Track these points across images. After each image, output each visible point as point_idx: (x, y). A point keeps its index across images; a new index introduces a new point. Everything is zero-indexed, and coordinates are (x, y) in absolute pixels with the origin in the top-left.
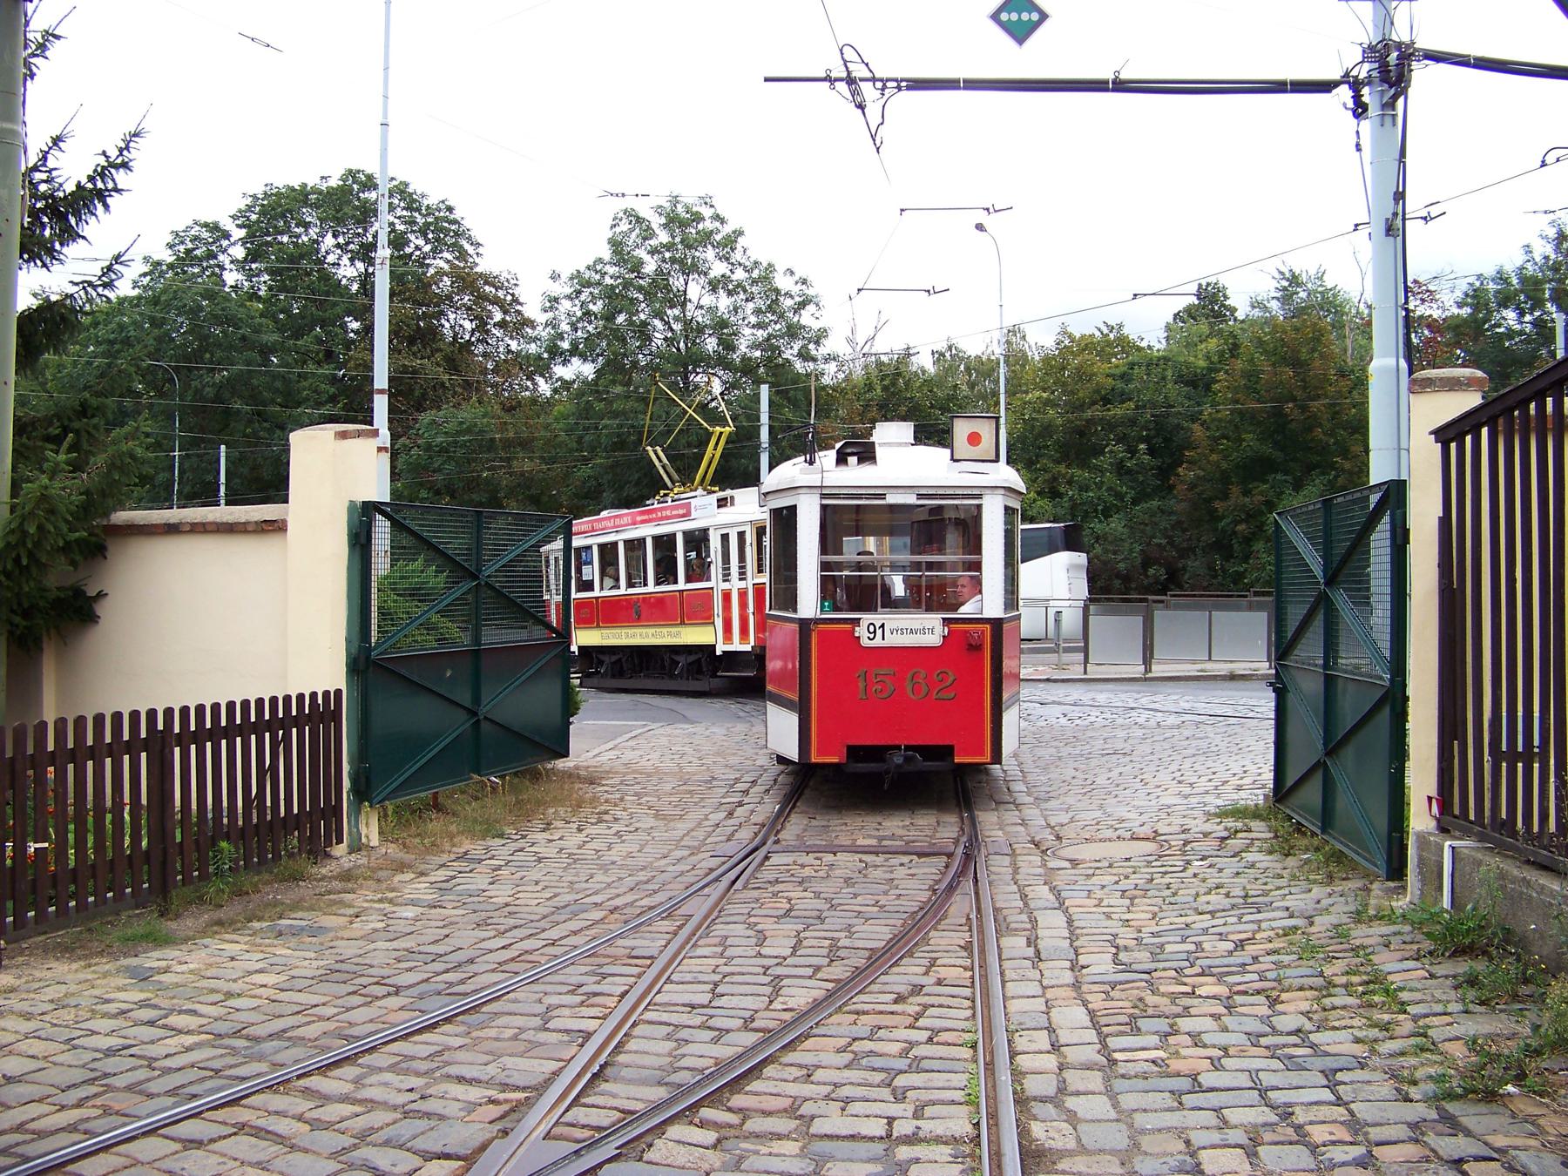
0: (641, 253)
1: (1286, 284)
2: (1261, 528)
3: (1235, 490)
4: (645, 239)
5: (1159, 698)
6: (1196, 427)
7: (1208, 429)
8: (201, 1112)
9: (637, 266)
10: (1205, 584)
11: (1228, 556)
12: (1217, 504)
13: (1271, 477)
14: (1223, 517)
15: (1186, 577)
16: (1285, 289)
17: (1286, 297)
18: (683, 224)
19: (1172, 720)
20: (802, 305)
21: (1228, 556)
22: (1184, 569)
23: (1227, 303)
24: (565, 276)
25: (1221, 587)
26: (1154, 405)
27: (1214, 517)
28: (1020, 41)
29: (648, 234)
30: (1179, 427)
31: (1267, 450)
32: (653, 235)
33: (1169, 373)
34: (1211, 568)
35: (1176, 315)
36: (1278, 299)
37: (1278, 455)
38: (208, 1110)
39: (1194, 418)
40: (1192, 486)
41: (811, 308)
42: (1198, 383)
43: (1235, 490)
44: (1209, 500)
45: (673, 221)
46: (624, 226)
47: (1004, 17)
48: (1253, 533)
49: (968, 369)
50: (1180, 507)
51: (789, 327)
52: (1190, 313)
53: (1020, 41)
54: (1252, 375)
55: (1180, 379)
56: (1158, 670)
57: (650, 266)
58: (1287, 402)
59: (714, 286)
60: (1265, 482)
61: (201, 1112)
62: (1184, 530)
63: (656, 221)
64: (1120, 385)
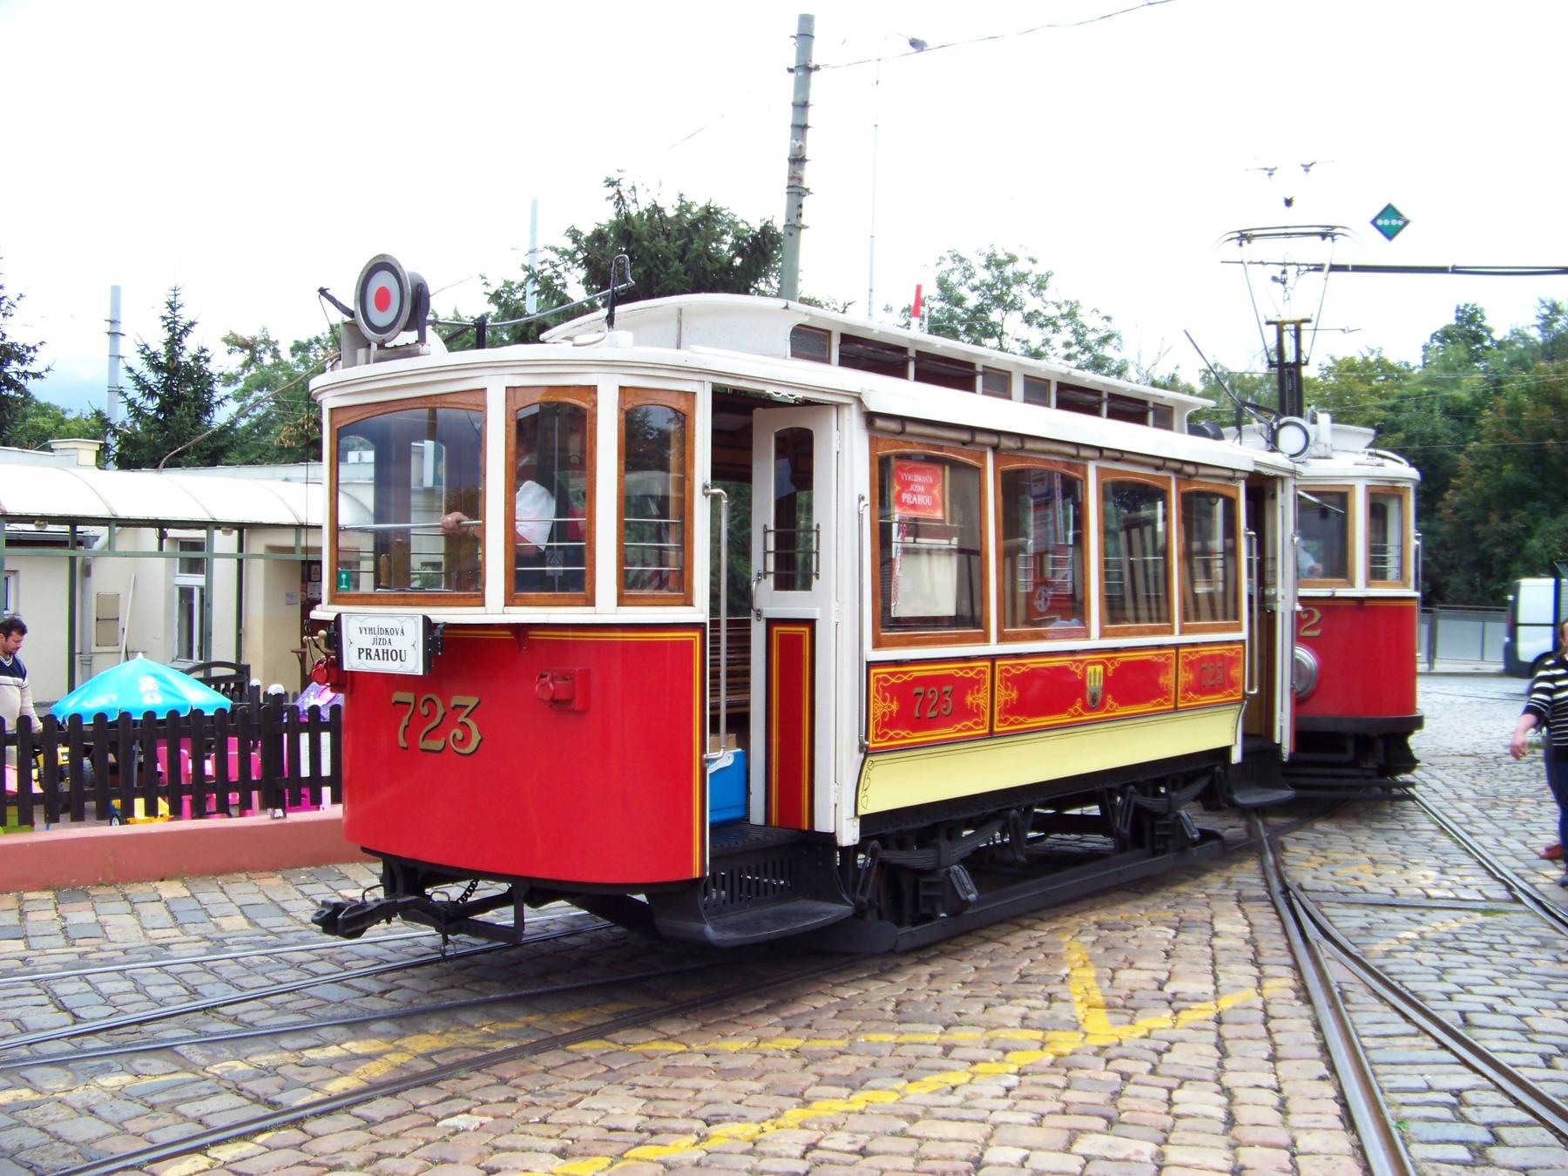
0: (963, 291)
1: (1546, 312)
2: (1519, 549)
3: (1494, 518)
4: (967, 278)
5: (1444, 687)
6: (1461, 456)
7: (1472, 459)
8: (302, 1119)
9: (959, 301)
10: (1466, 598)
11: (1488, 575)
12: (1477, 528)
13: (1529, 505)
14: (1483, 539)
15: (1449, 591)
16: (1545, 317)
17: (1547, 323)
18: (999, 265)
19: (1462, 700)
20: (1105, 340)
21: (1488, 575)
22: (1447, 584)
23: (1484, 324)
24: (898, 309)
25: (1480, 601)
26: (1422, 437)
27: (1475, 539)
28: (1390, 237)
29: (968, 273)
30: (1443, 456)
31: (1527, 480)
32: (972, 275)
33: (1437, 407)
34: (1471, 584)
35: (1434, 336)
36: (1538, 326)
37: (1535, 485)
38: (316, 1115)
39: (1459, 450)
40: (1456, 511)
41: (1114, 341)
42: (1462, 415)
43: (1494, 518)
44: (1471, 524)
45: (993, 262)
46: (948, 265)
47: (1380, 222)
48: (1512, 556)
49: (1232, 387)
50: (1445, 529)
51: (1096, 357)
52: (1446, 335)
53: (1390, 237)
54: (1515, 409)
55: (1447, 412)
56: (1439, 667)
57: (972, 301)
58: (1546, 439)
59: (1028, 319)
60: (1524, 509)
61: (302, 1119)
62: (1448, 550)
63: (978, 262)
64: (1390, 416)
